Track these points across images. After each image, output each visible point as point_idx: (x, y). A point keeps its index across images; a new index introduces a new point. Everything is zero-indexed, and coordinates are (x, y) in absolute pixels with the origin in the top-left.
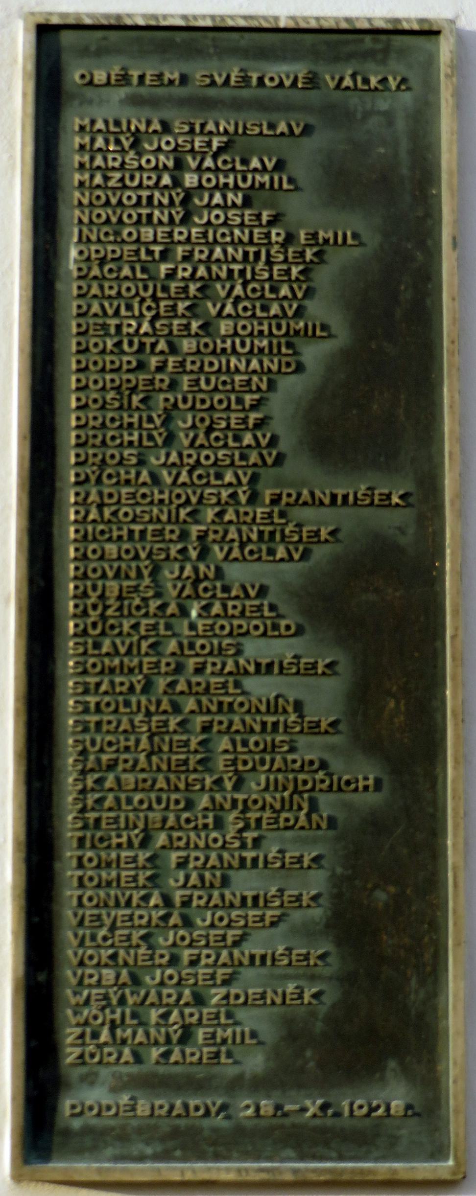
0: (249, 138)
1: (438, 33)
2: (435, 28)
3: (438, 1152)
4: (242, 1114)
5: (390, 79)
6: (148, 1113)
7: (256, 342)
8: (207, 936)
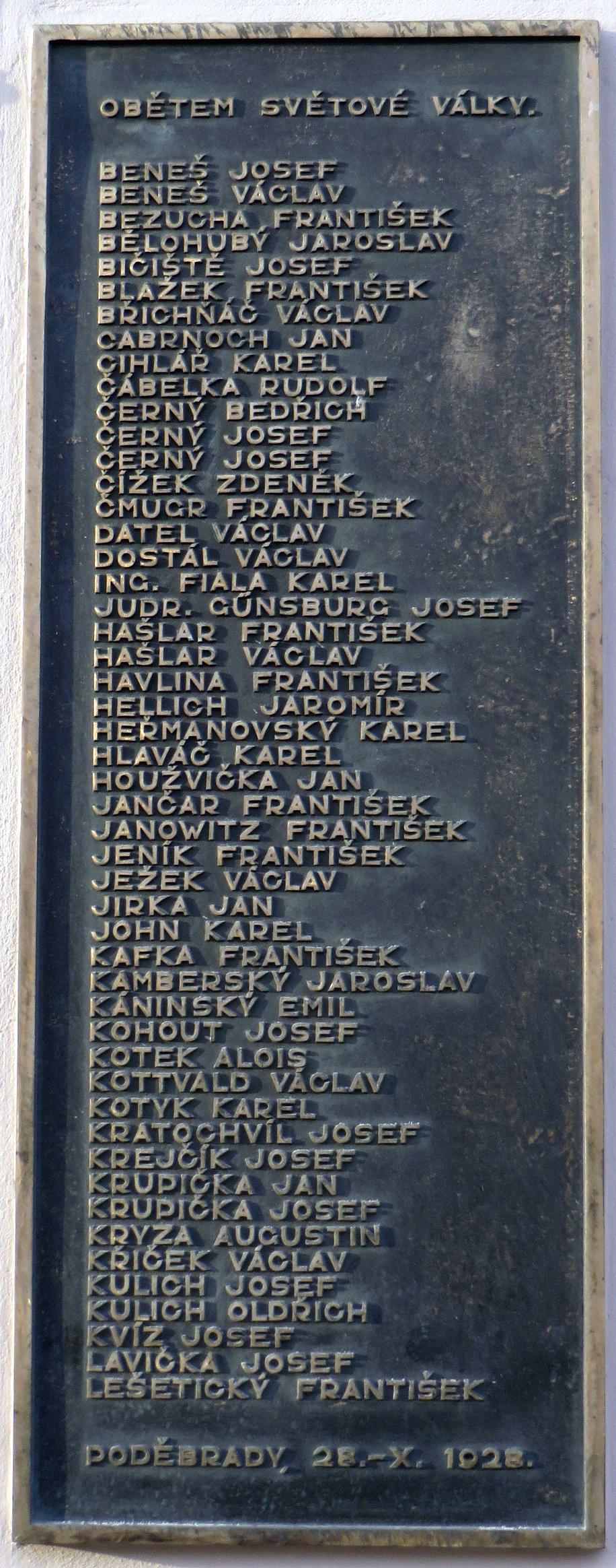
0: (460, 621)
1: (576, 39)
2: (571, 31)
3: (572, 1510)
4: (315, 1463)
5: (512, 99)
6: (192, 1462)
7: (355, 700)
8: (287, 431)
